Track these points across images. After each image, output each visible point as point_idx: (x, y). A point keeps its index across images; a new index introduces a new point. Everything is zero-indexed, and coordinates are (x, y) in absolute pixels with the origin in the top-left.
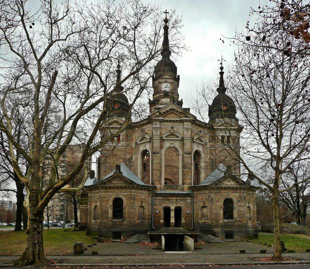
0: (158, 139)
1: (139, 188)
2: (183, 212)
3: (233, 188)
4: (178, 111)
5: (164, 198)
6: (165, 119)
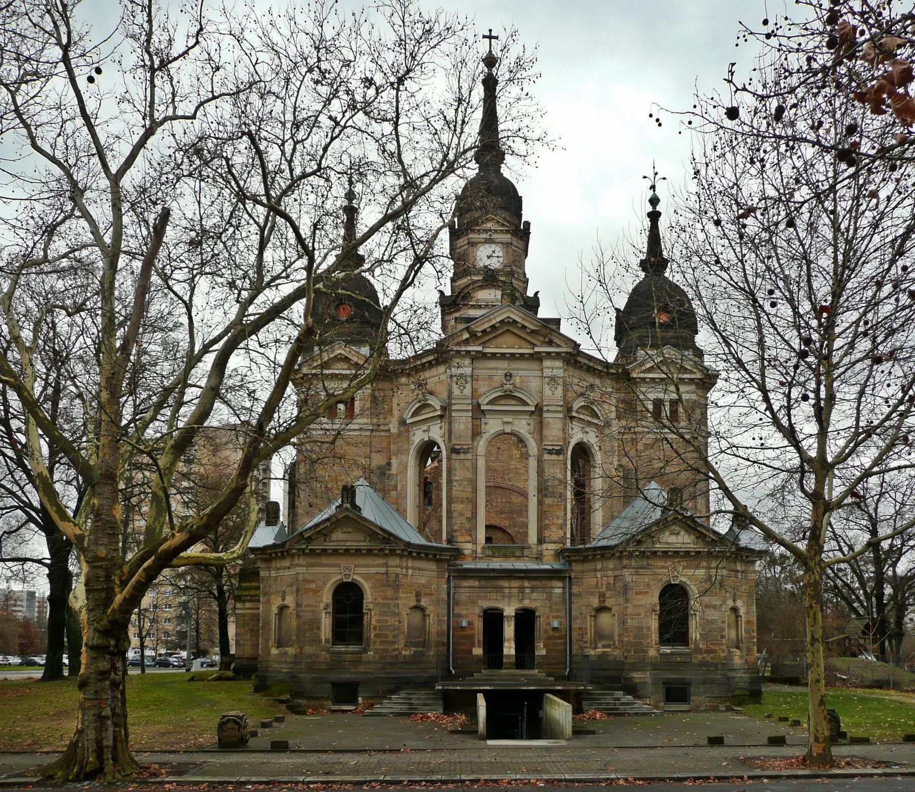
1: (410, 553)
2: (541, 625)
3: (687, 553)
5: (483, 583)
6: (487, 350)
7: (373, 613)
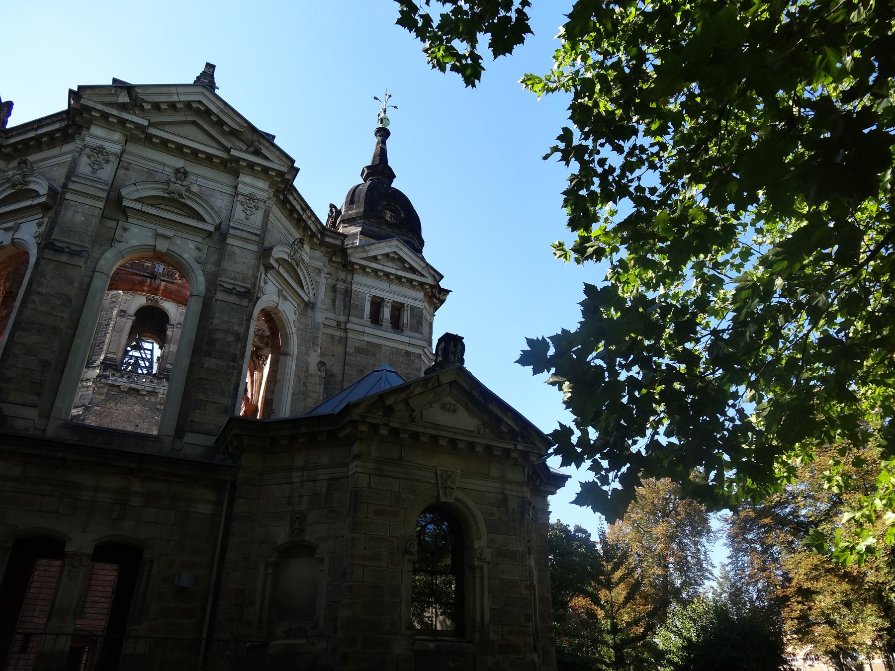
3: (471, 445)
4: (220, 123)
6: (152, 131)
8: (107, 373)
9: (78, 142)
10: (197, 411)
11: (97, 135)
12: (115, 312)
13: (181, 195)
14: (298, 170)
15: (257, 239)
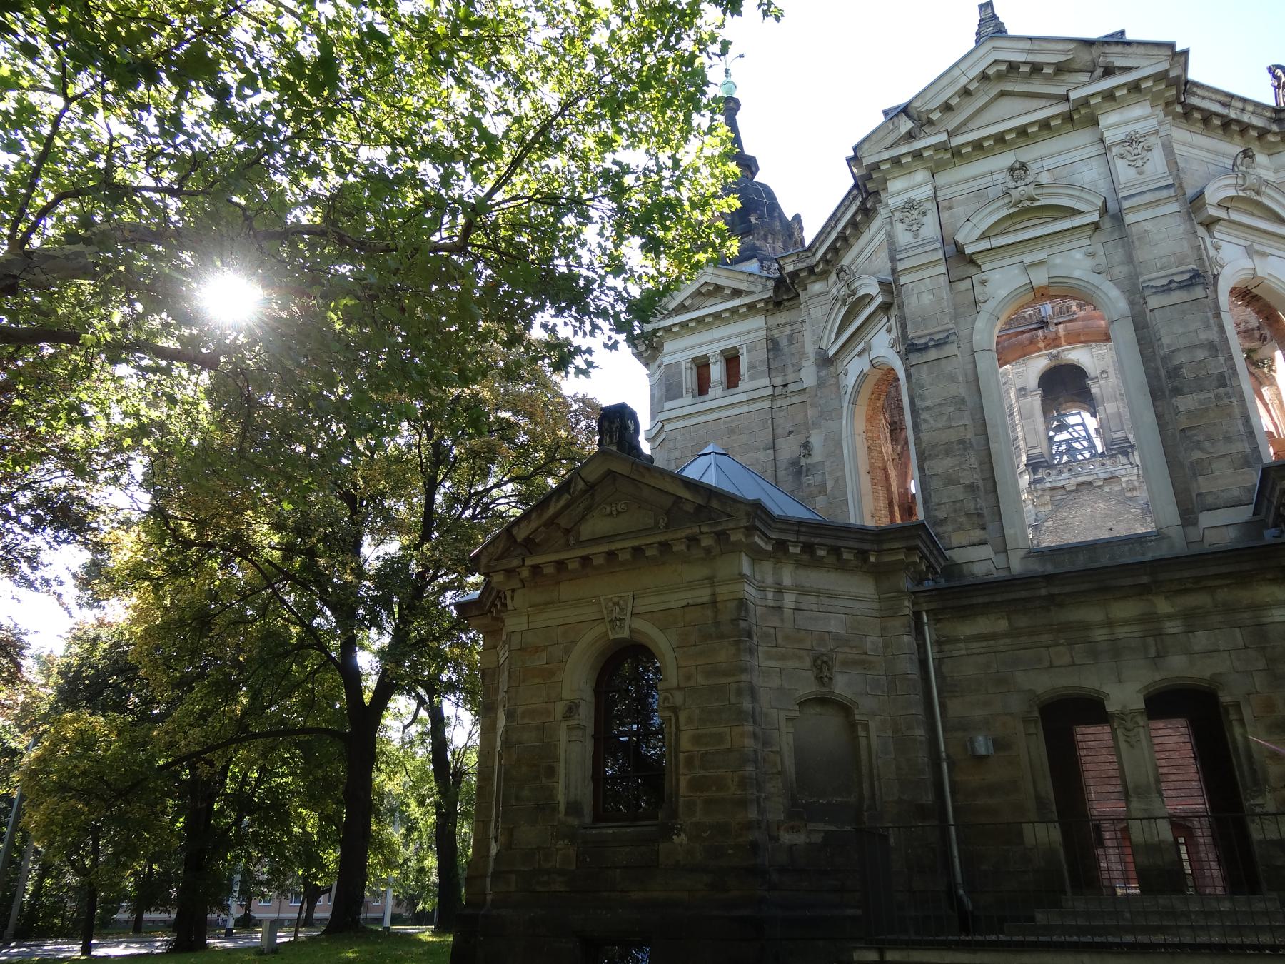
0: (934, 263)
4: (1036, 68)
5: (1022, 621)
6: (956, 141)
7: (683, 716)
8: (1039, 476)
9: (882, 211)
10: (1200, 479)
11: (904, 188)
12: (1013, 395)
13: (1031, 199)
14: (1186, 53)
15: (1172, 192)
